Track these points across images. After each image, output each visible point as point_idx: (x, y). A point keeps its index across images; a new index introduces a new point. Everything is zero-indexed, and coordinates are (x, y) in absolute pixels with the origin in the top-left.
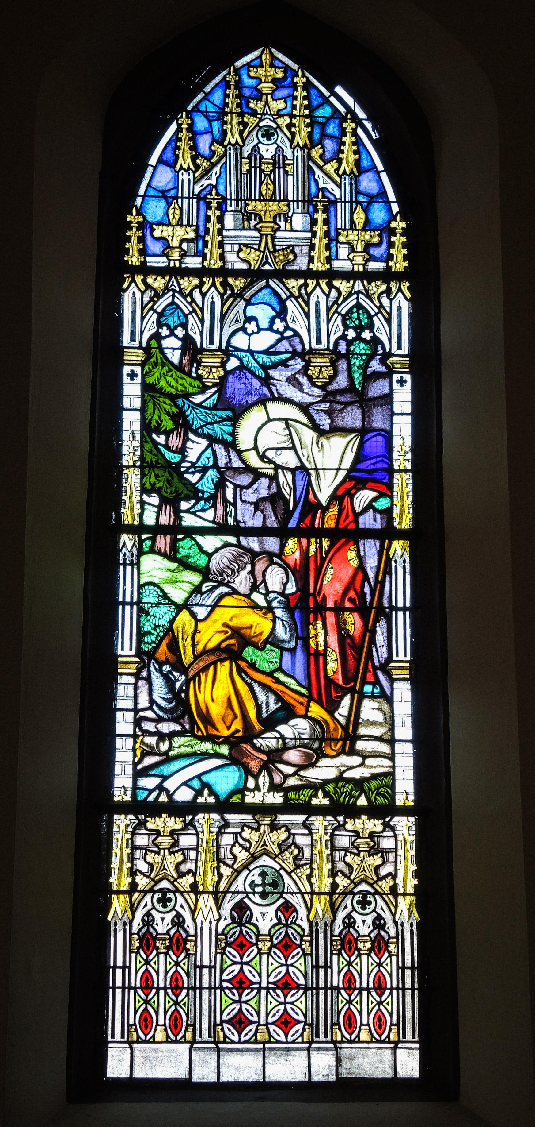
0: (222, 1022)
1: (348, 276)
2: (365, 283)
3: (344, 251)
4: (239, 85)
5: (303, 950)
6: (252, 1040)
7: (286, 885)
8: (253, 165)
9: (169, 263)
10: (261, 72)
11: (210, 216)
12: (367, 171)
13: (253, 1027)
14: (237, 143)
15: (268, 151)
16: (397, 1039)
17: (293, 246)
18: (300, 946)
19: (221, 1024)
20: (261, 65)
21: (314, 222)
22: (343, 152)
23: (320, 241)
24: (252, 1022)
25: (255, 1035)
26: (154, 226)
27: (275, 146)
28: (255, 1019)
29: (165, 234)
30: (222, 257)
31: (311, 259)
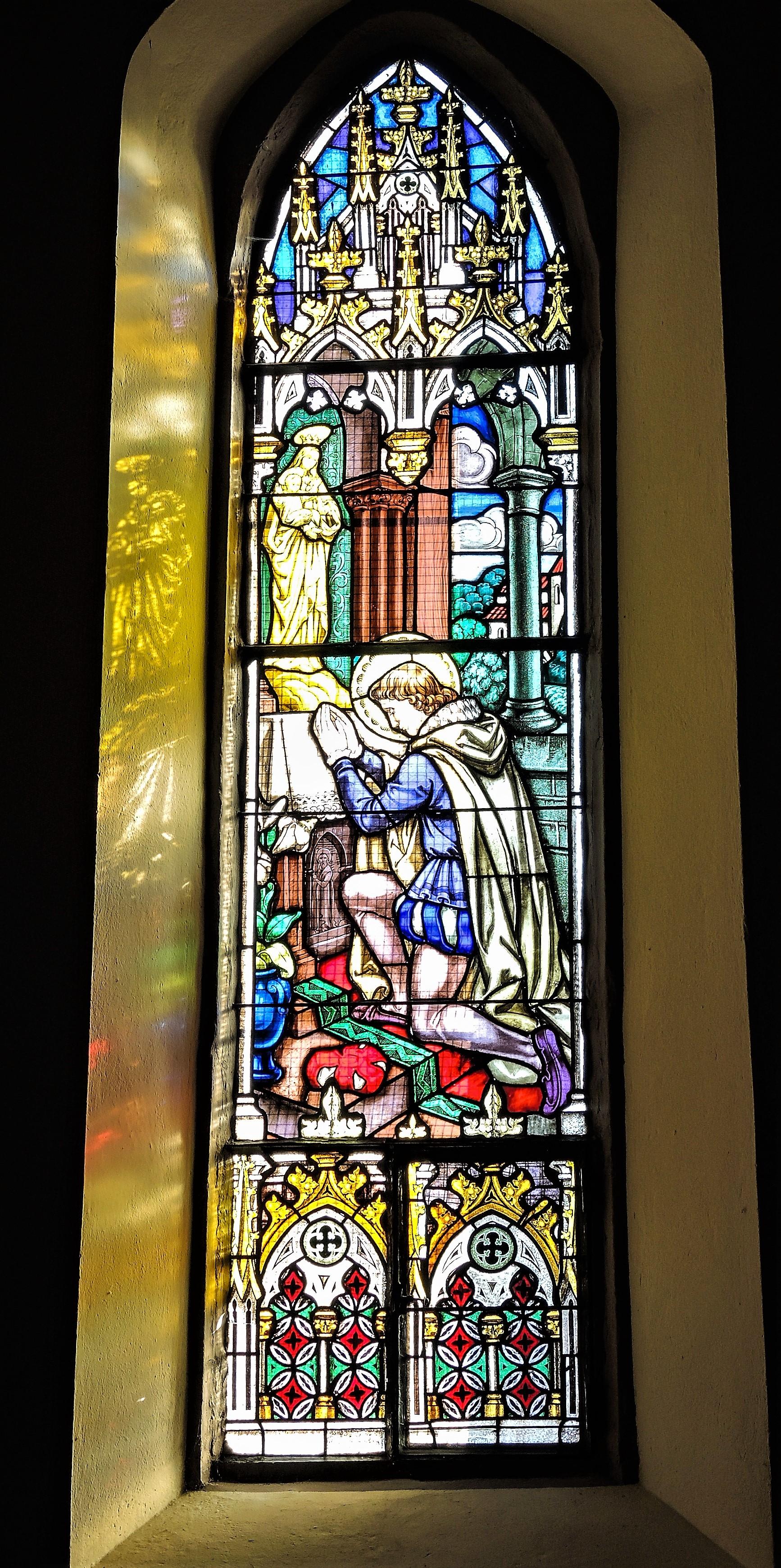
4: (370, 118)
6: (309, 1417)
7: (519, 1244)
10: (398, 94)
20: (398, 84)
25: (312, 1411)
27: (417, 196)
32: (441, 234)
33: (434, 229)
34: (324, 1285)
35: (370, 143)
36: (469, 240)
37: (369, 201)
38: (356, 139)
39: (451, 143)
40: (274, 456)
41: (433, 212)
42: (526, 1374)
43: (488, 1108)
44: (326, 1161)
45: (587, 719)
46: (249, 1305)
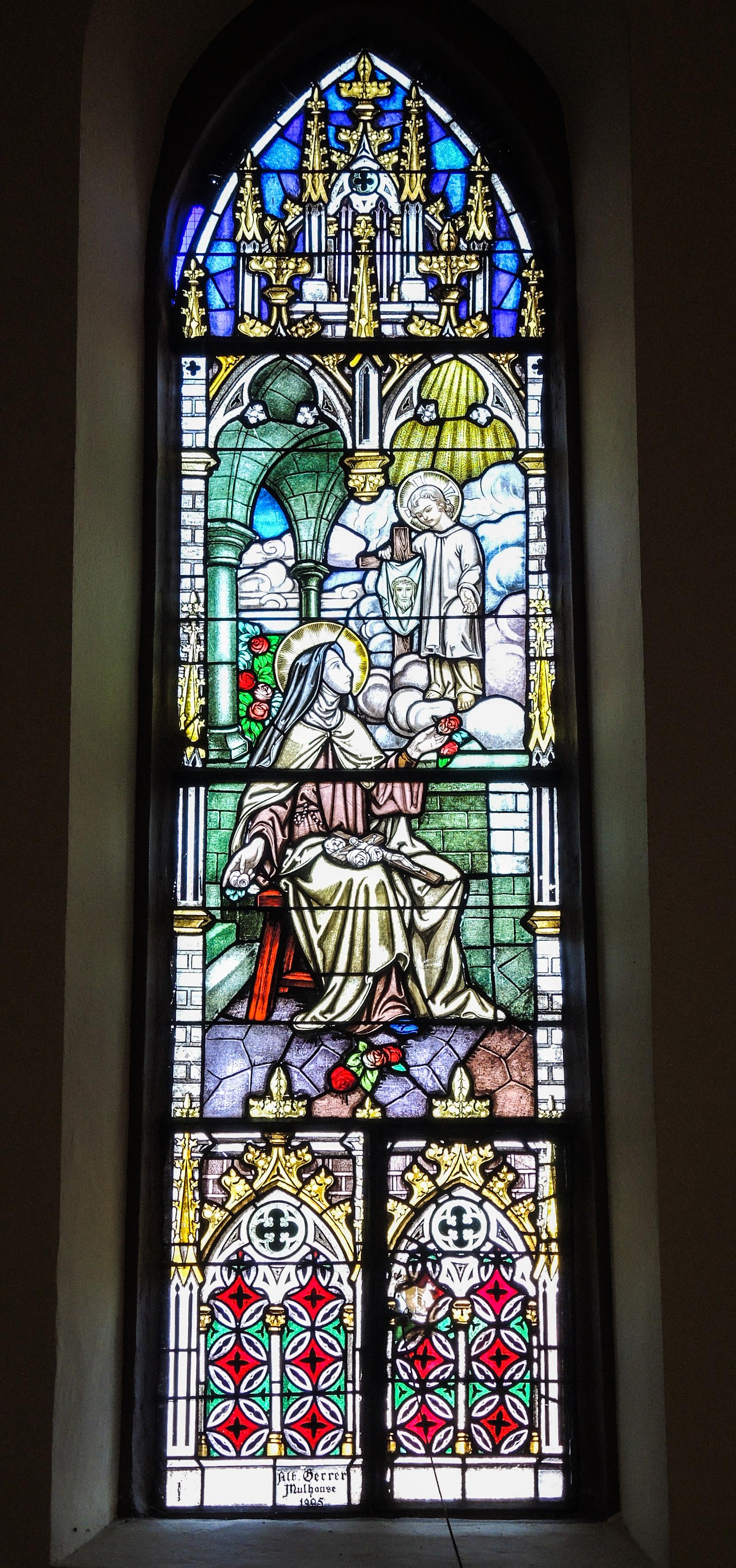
0: (396, 1428)
10: (356, 90)
14: (254, 238)
15: (364, 204)
20: (357, 79)
27: (375, 197)
32: (401, 238)
34: (277, 1282)
36: (431, 247)
37: (320, 200)
39: (413, 139)
40: (205, 473)
41: (394, 215)
42: (499, 1380)
44: (277, 1138)
46: (191, 1288)
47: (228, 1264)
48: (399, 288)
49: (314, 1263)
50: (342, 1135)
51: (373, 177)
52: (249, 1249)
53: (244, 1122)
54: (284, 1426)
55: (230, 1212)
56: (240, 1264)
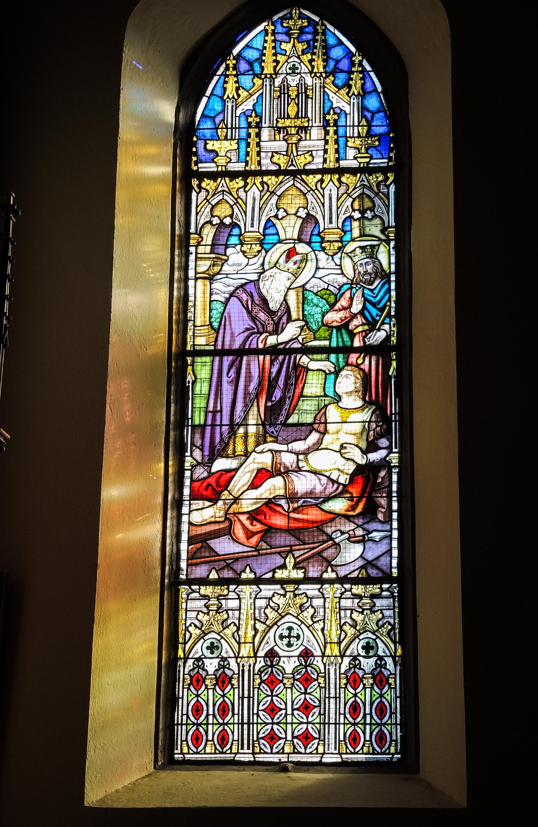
1: (353, 171)
2: (367, 175)
3: (351, 153)
5: (319, 683)
8: (300, 92)
9: (360, 165)
10: (291, 22)
11: (250, 133)
12: (370, 93)
13: (282, 741)
16: (236, 752)
17: (311, 151)
18: (281, 681)
19: (257, 740)
21: (327, 133)
22: (352, 79)
23: (331, 147)
24: (281, 738)
26: (208, 142)
28: (283, 736)
29: (215, 148)
30: (259, 163)
31: (325, 160)
33: (309, 95)
35: (273, 44)
38: (267, 43)
43: (288, 564)
45: (256, 480)
47: (266, 656)
48: (310, 132)
49: (306, 654)
50: (319, 586)
51: (289, 71)
52: (276, 648)
53: (272, 581)
54: (293, 737)
55: (203, 632)
56: (272, 654)
